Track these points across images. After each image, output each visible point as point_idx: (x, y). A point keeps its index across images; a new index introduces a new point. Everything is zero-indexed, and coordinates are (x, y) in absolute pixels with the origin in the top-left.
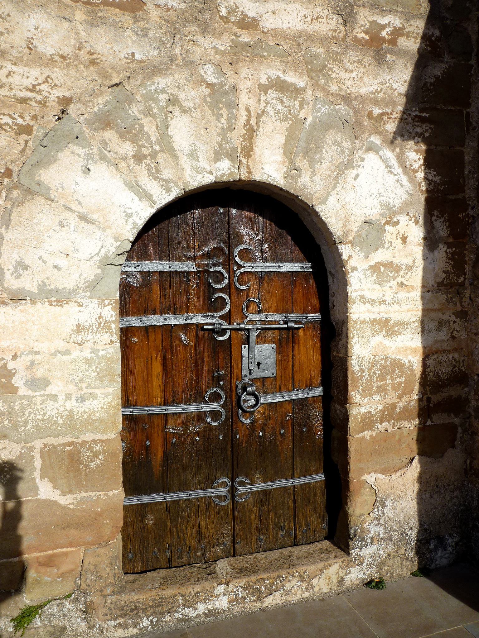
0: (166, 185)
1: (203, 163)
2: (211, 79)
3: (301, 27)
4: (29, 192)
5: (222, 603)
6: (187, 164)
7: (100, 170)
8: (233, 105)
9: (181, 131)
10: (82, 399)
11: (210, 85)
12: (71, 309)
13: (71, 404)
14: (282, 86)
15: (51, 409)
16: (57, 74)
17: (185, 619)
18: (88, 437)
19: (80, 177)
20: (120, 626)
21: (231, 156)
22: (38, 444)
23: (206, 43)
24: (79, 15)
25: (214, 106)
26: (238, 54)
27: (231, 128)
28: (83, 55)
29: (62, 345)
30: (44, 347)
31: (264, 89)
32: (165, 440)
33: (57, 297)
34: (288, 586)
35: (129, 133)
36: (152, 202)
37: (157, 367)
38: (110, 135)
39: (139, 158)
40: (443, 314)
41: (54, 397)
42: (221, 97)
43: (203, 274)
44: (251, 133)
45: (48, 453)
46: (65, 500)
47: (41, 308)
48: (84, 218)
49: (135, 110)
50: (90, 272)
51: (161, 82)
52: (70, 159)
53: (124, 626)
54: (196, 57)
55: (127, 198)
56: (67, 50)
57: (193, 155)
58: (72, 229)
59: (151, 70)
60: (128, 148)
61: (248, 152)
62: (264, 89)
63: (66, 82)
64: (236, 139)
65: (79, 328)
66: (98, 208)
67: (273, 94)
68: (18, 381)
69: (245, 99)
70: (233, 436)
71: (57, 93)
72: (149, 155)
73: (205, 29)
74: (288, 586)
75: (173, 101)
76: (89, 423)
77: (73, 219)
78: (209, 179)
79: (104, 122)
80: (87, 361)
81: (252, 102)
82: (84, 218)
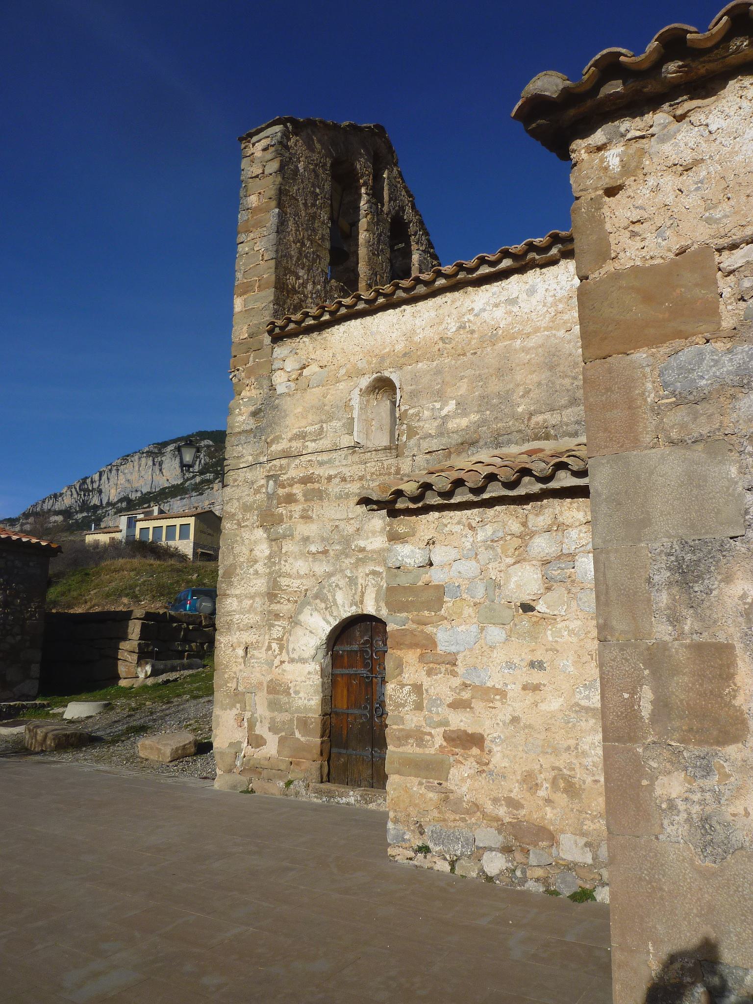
0: (335, 618)
1: (347, 608)
2: (349, 575)
3: (382, 546)
4: (297, 623)
5: (352, 800)
6: (341, 609)
7: (315, 614)
8: (356, 584)
9: (340, 597)
10: (309, 700)
11: (349, 577)
12: (307, 665)
13: (306, 701)
14: (374, 573)
15: (300, 703)
16: (304, 581)
17: (338, 803)
18: (310, 715)
19: (309, 617)
20: (316, 797)
21: (356, 605)
22: (296, 715)
23: (347, 561)
24: (310, 559)
25: (350, 585)
26: (360, 562)
27: (355, 594)
28: (311, 573)
29: (304, 679)
30: (299, 679)
31: (367, 575)
32: (348, 727)
33: (303, 661)
34: (379, 802)
35: (324, 600)
36: (331, 625)
37: (345, 692)
38: (318, 601)
39: (326, 609)
40: (429, 673)
41: (301, 698)
42: (352, 581)
43: (362, 651)
44: (363, 594)
45: (298, 719)
46: (302, 739)
47: (299, 664)
48: (311, 632)
49: (325, 591)
50: (313, 652)
51: (333, 579)
52: (307, 610)
53: (317, 798)
54: (344, 568)
55: (323, 624)
56: (307, 572)
57: (343, 606)
58: (573, 570)
59: (330, 575)
60: (323, 605)
61: (362, 602)
62: (367, 575)
63: (308, 583)
64: (357, 598)
65: (309, 673)
66: (318, 626)
67: (371, 576)
68: (291, 691)
69: (360, 581)
70: (372, 728)
71: (305, 588)
72: (330, 606)
73: (347, 556)
74: (379, 802)
75: (337, 586)
76: (311, 710)
77: (308, 632)
78: (349, 614)
79: (316, 597)
80: (311, 686)
81: (363, 582)
82: (311, 632)
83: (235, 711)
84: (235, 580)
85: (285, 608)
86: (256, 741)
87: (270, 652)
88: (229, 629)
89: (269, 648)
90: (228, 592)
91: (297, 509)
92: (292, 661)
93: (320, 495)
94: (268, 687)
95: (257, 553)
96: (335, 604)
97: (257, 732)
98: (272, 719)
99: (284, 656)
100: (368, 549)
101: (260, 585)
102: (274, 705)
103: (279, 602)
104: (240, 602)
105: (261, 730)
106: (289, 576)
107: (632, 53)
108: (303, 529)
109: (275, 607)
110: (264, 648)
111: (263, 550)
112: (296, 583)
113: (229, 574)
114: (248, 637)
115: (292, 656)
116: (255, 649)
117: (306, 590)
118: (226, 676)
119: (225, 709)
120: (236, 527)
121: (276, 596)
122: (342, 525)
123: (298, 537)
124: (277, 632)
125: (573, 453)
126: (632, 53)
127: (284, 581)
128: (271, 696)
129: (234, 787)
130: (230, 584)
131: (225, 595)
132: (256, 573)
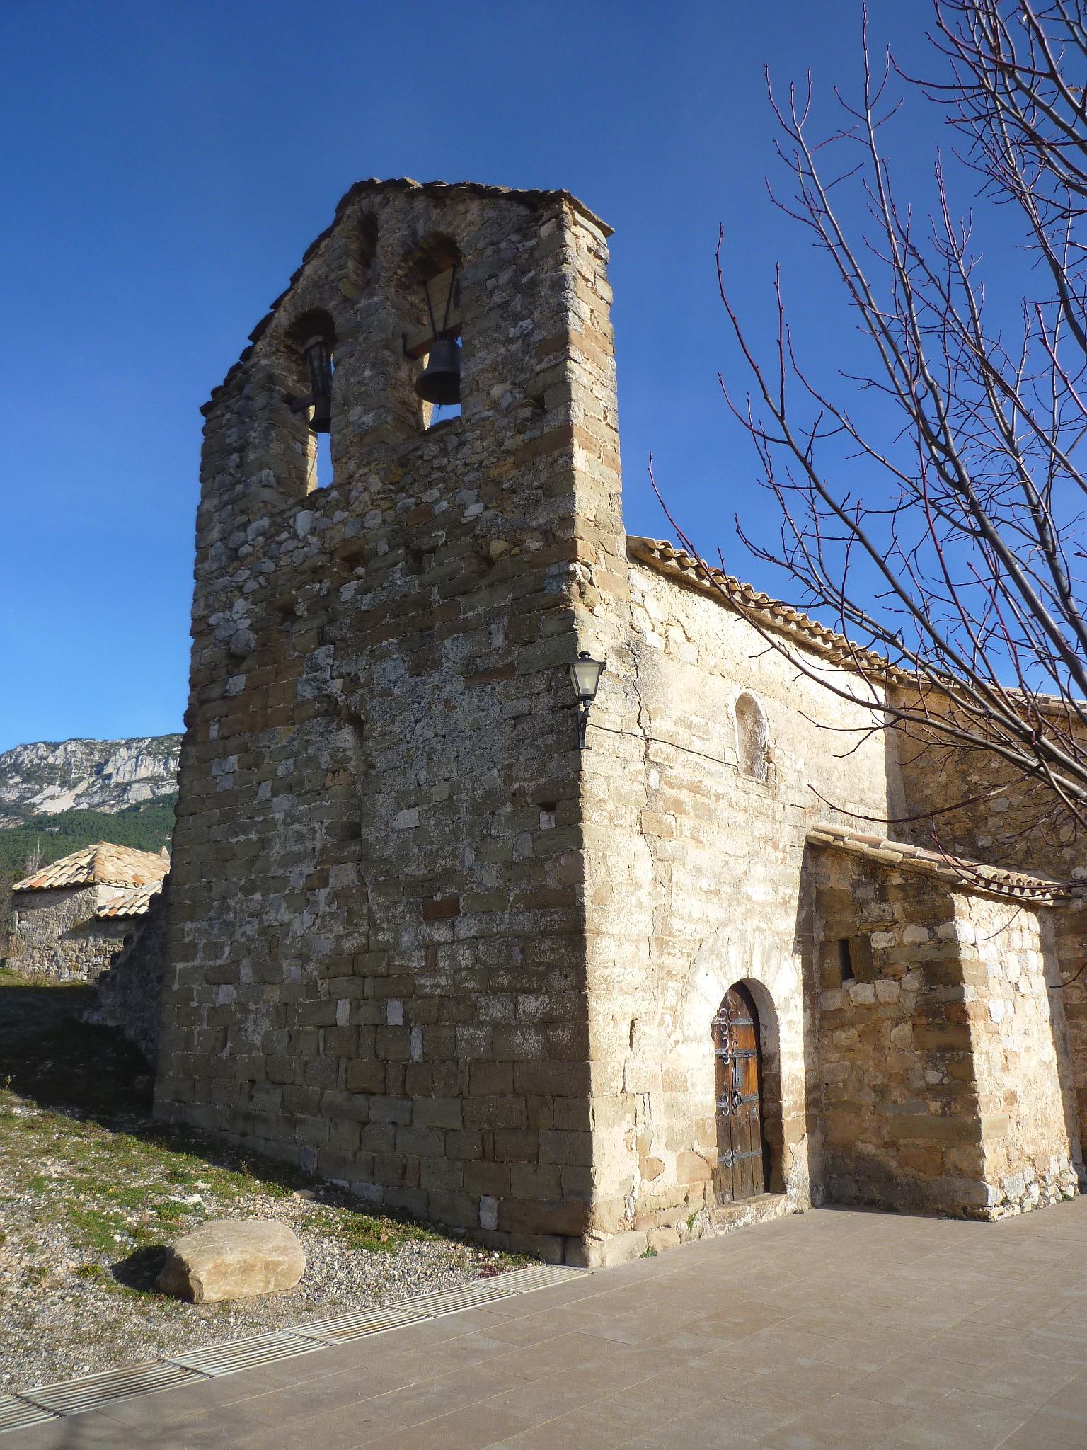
5: (748, 1219)
42: (743, 934)
60: (718, 964)
63: (703, 931)
68: (689, 1084)
71: (699, 937)
83: (625, 1126)
84: (611, 909)
85: (678, 963)
86: (652, 1169)
87: (663, 1028)
88: (609, 991)
89: (662, 1022)
90: (603, 928)
91: (687, 822)
92: (686, 1040)
93: (707, 814)
94: (664, 1081)
95: (637, 873)
96: (728, 963)
97: (653, 1155)
98: (671, 1129)
99: (678, 1035)
100: (754, 898)
101: (644, 924)
102: (671, 1107)
103: (669, 954)
104: (619, 946)
105: (658, 1151)
106: (680, 916)
107: (615, 425)
108: (696, 856)
109: (667, 960)
110: (657, 1021)
111: (645, 870)
112: (689, 929)
113: (600, 901)
114: (635, 1005)
115: (687, 1033)
116: (646, 1023)
117: (701, 940)
118: (610, 1070)
119: (612, 1126)
120: (606, 822)
121: (666, 943)
122: (732, 860)
123: (689, 865)
124: (671, 998)
125: (1004, 718)
126: (615, 425)
127: (676, 924)
128: (668, 1095)
129: (631, 1254)
130: (606, 915)
131: (599, 932)
132: (640, 904)
